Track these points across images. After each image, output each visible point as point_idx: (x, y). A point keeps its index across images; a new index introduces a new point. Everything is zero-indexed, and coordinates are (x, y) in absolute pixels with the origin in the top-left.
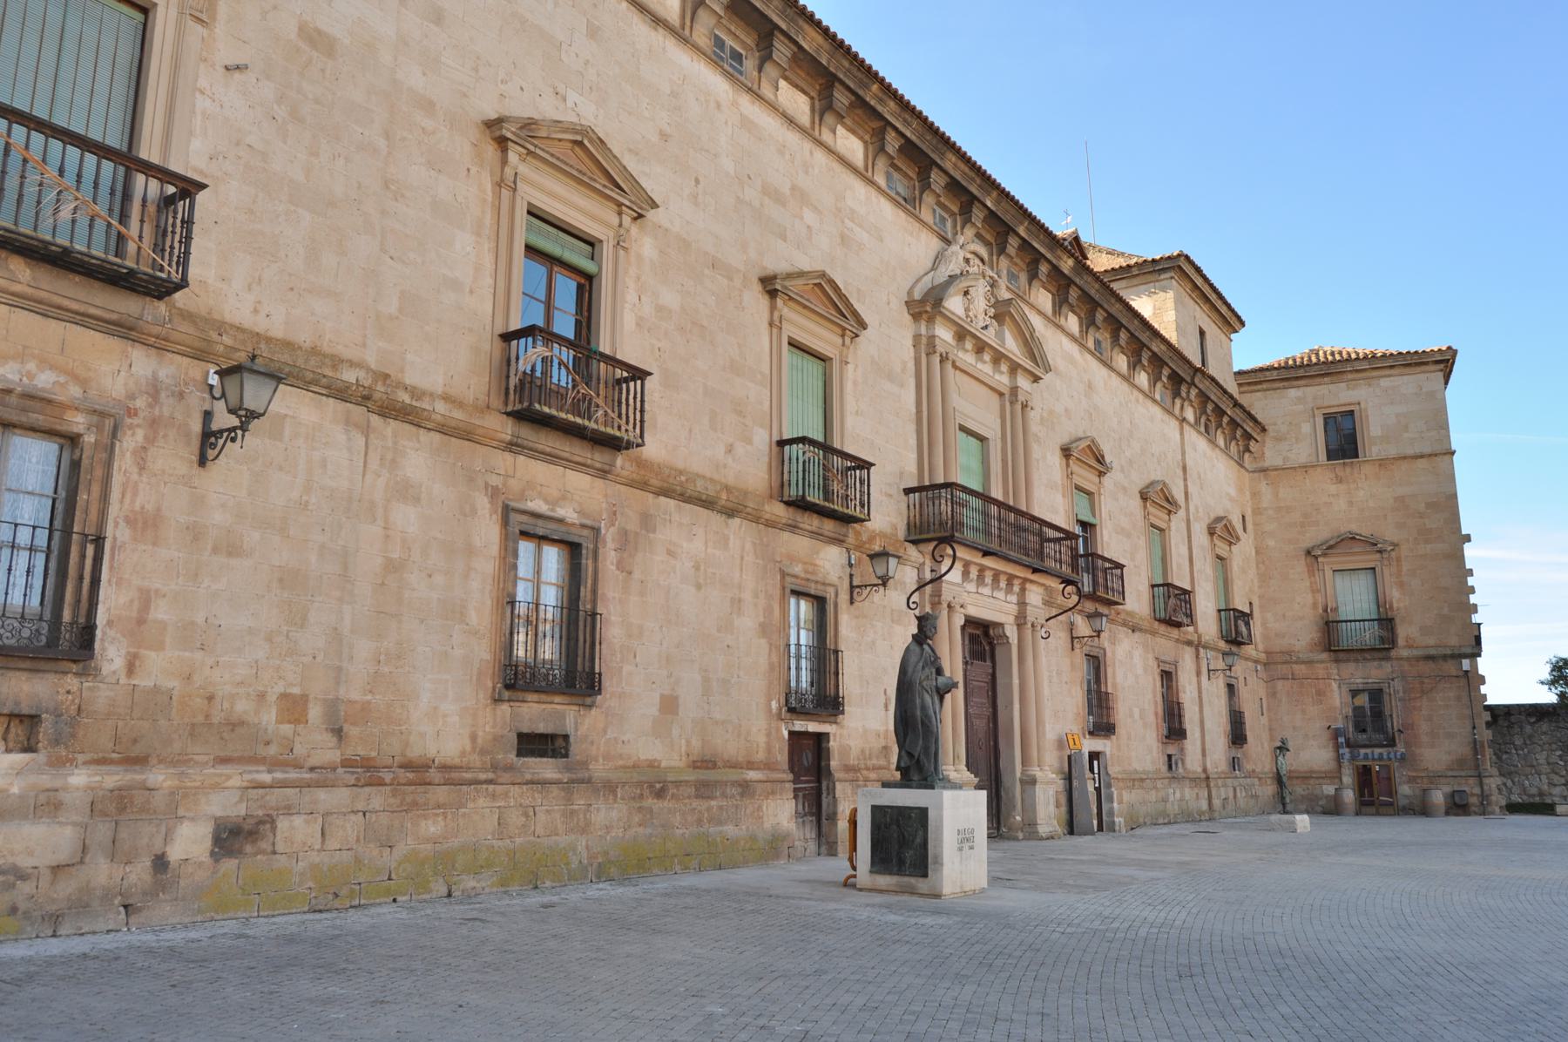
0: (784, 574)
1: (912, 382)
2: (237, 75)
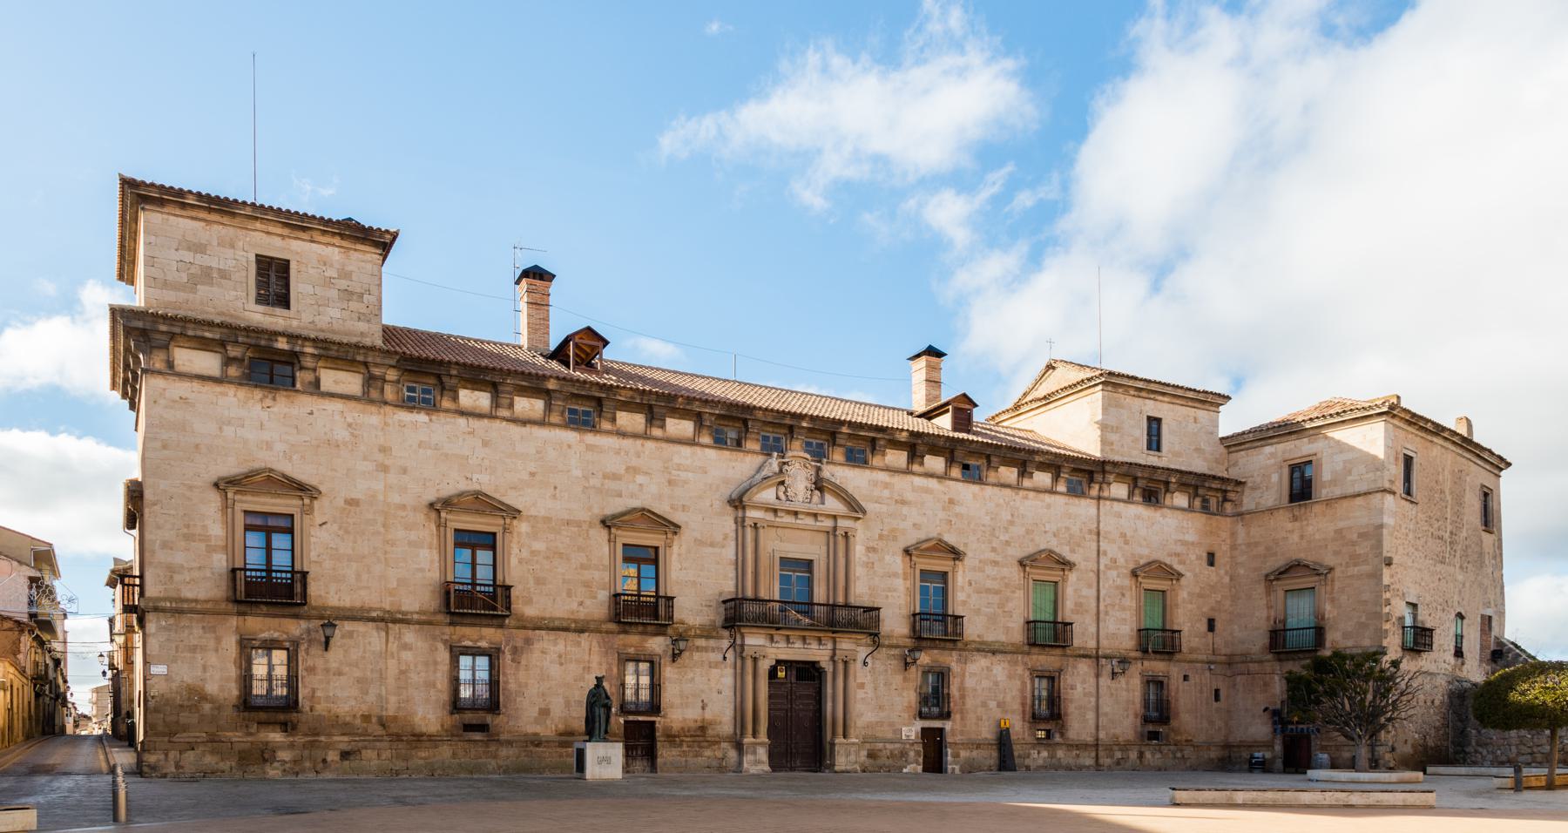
1: (733, 544)
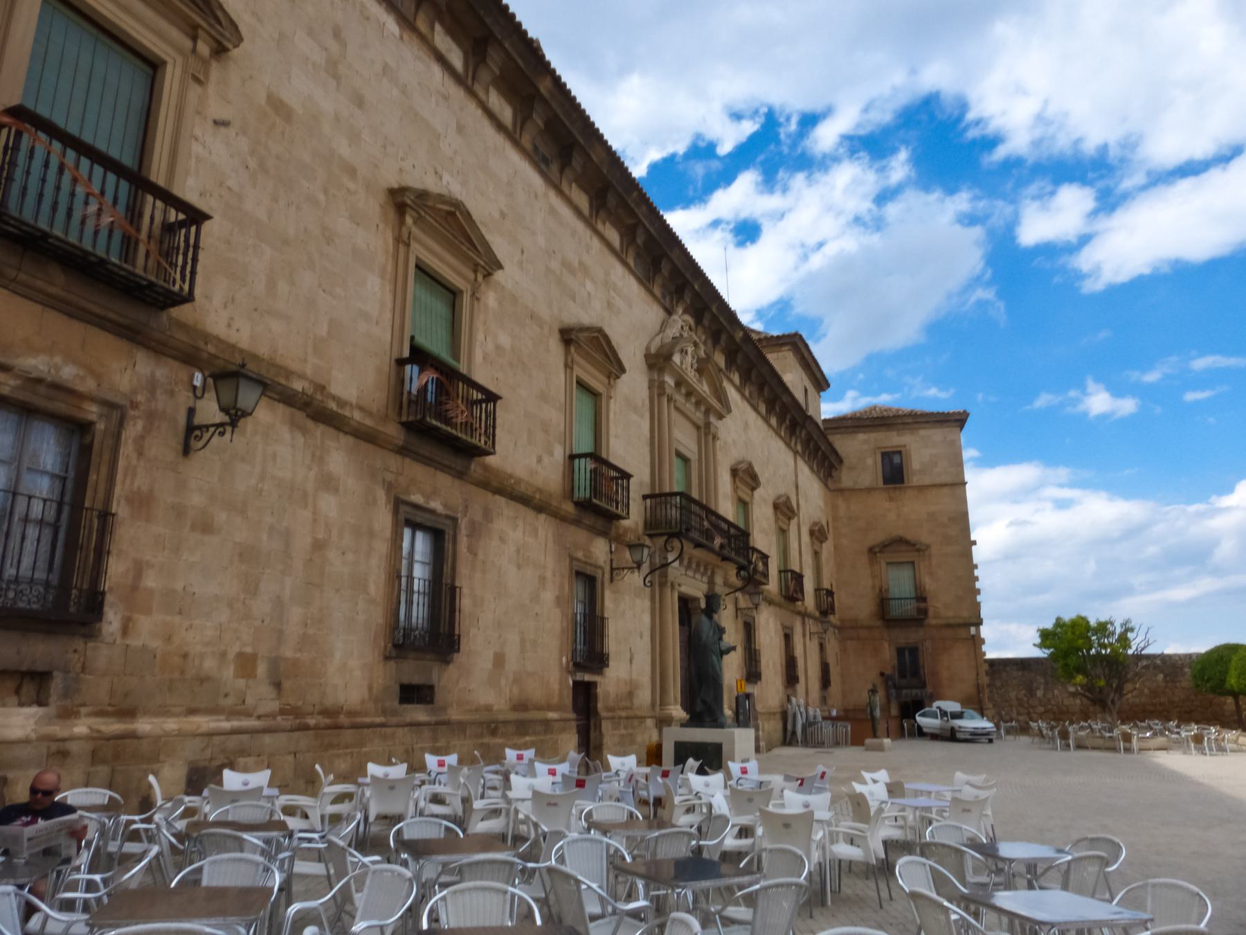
0: (572, 559)
2: (222, 130)
